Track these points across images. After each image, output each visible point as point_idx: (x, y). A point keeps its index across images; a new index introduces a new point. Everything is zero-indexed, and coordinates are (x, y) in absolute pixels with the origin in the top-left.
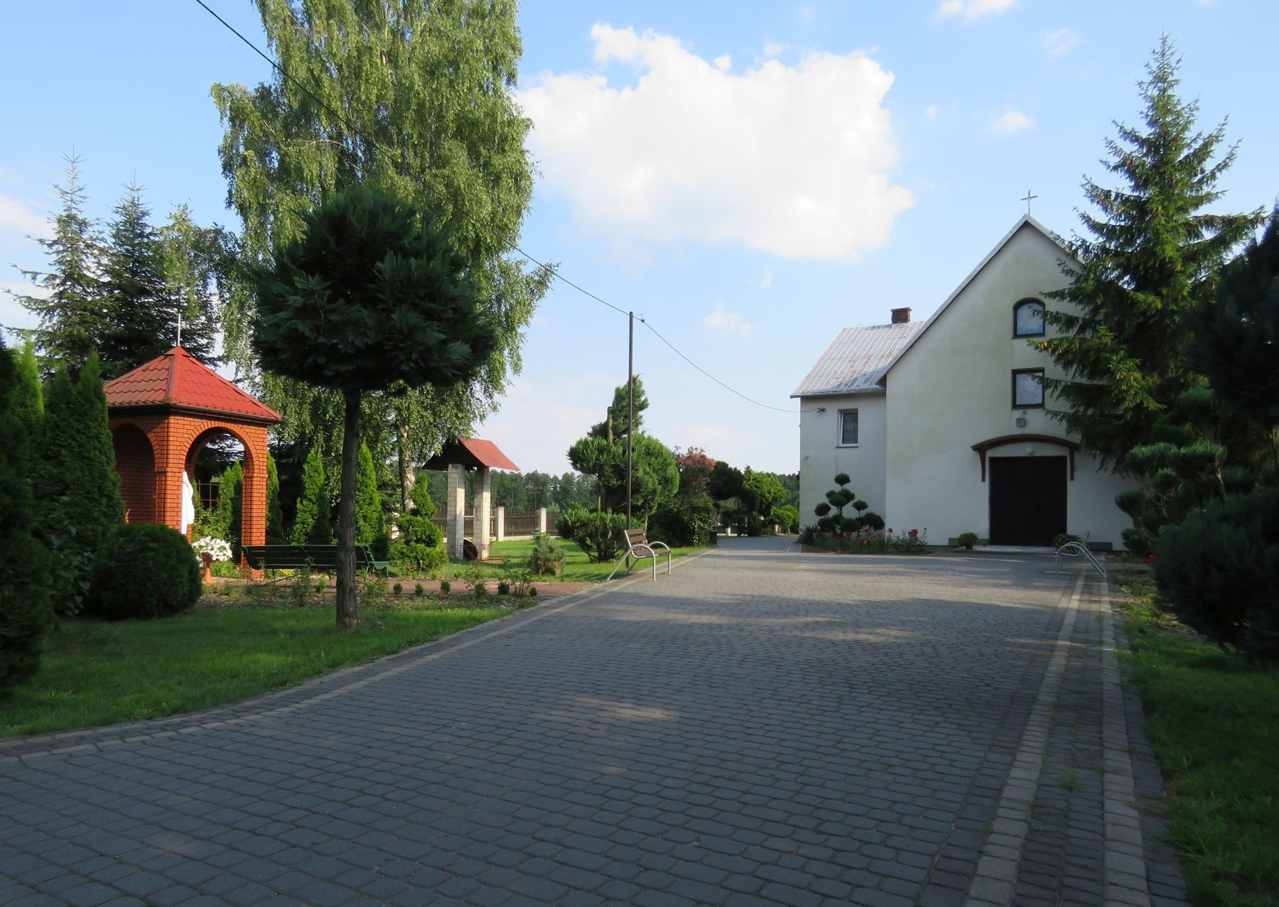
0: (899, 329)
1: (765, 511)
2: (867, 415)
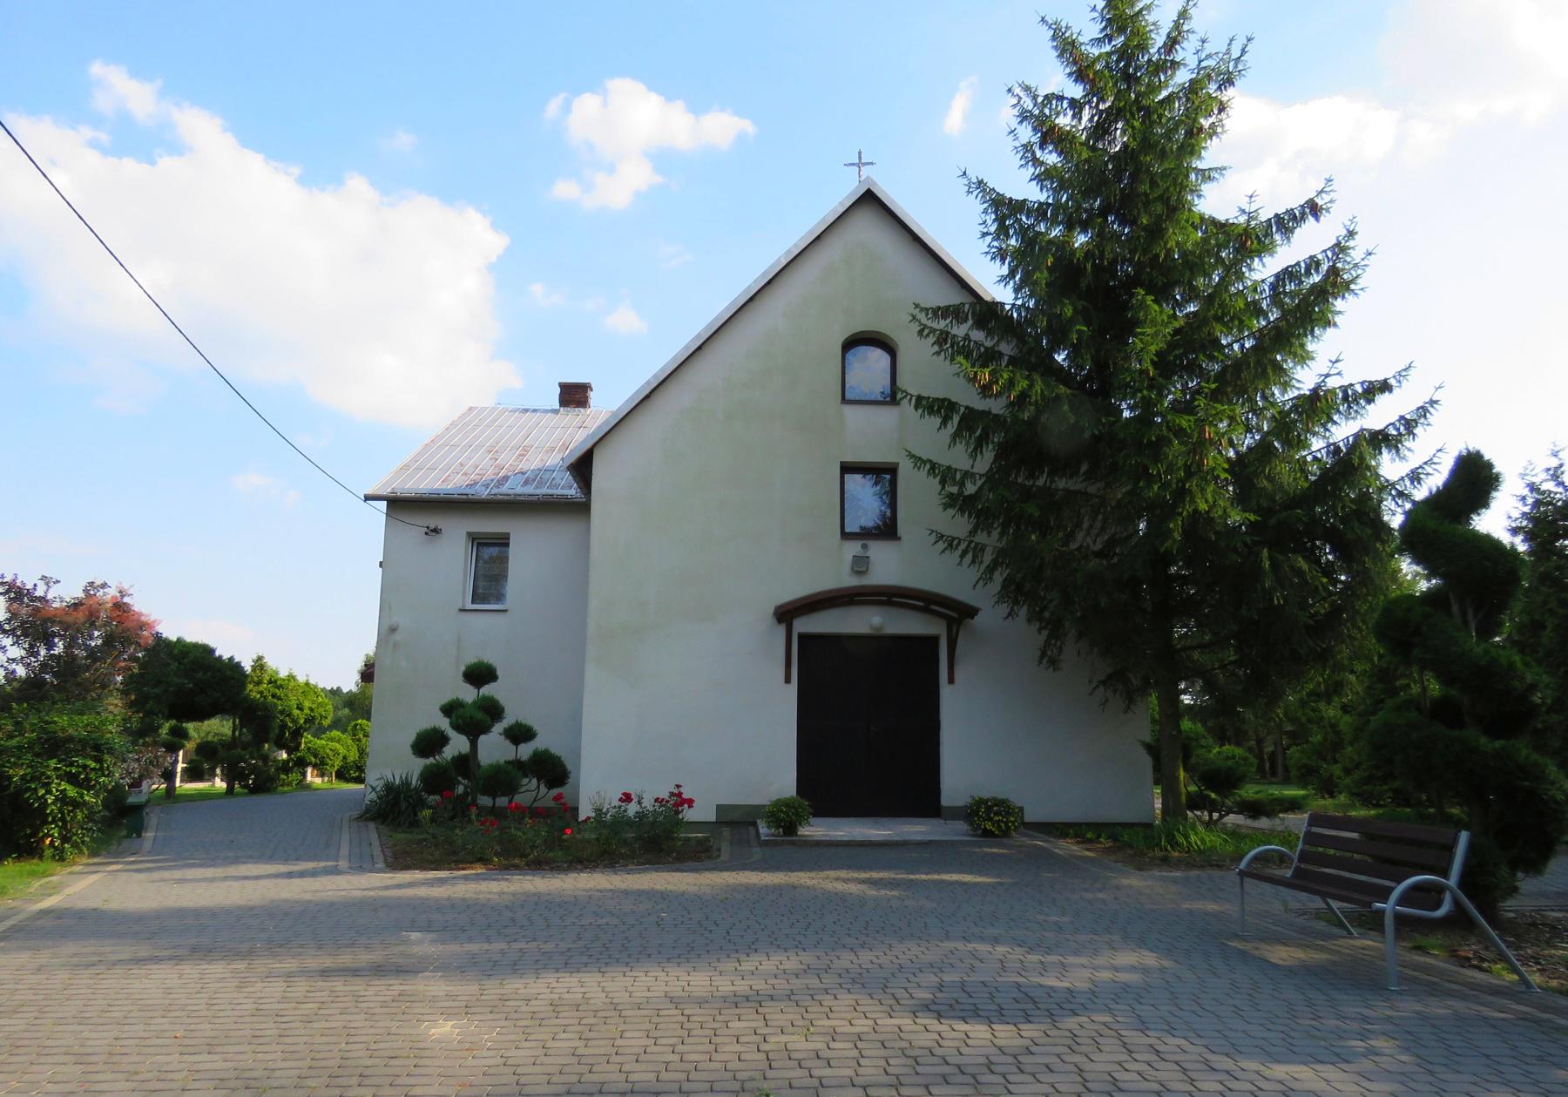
0: (572, 416)
1: (290, 739)
2: (532, 552)
